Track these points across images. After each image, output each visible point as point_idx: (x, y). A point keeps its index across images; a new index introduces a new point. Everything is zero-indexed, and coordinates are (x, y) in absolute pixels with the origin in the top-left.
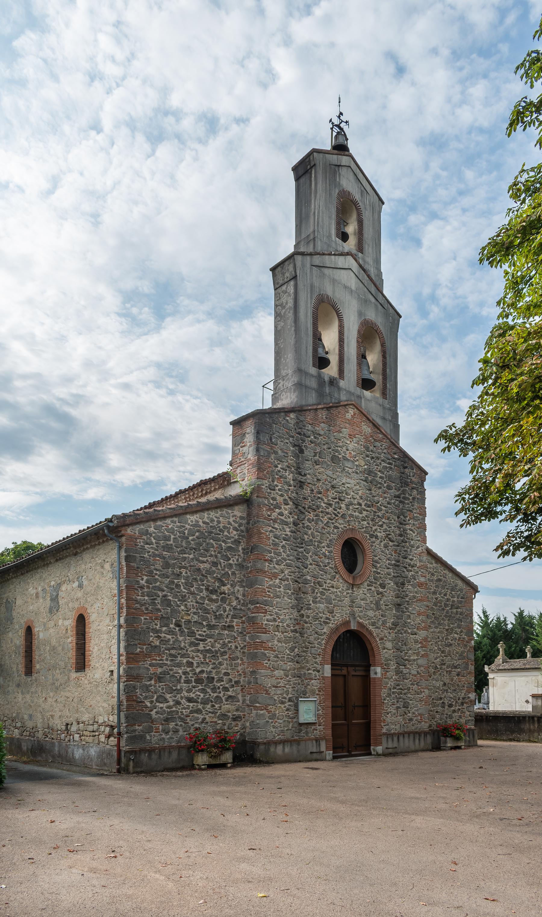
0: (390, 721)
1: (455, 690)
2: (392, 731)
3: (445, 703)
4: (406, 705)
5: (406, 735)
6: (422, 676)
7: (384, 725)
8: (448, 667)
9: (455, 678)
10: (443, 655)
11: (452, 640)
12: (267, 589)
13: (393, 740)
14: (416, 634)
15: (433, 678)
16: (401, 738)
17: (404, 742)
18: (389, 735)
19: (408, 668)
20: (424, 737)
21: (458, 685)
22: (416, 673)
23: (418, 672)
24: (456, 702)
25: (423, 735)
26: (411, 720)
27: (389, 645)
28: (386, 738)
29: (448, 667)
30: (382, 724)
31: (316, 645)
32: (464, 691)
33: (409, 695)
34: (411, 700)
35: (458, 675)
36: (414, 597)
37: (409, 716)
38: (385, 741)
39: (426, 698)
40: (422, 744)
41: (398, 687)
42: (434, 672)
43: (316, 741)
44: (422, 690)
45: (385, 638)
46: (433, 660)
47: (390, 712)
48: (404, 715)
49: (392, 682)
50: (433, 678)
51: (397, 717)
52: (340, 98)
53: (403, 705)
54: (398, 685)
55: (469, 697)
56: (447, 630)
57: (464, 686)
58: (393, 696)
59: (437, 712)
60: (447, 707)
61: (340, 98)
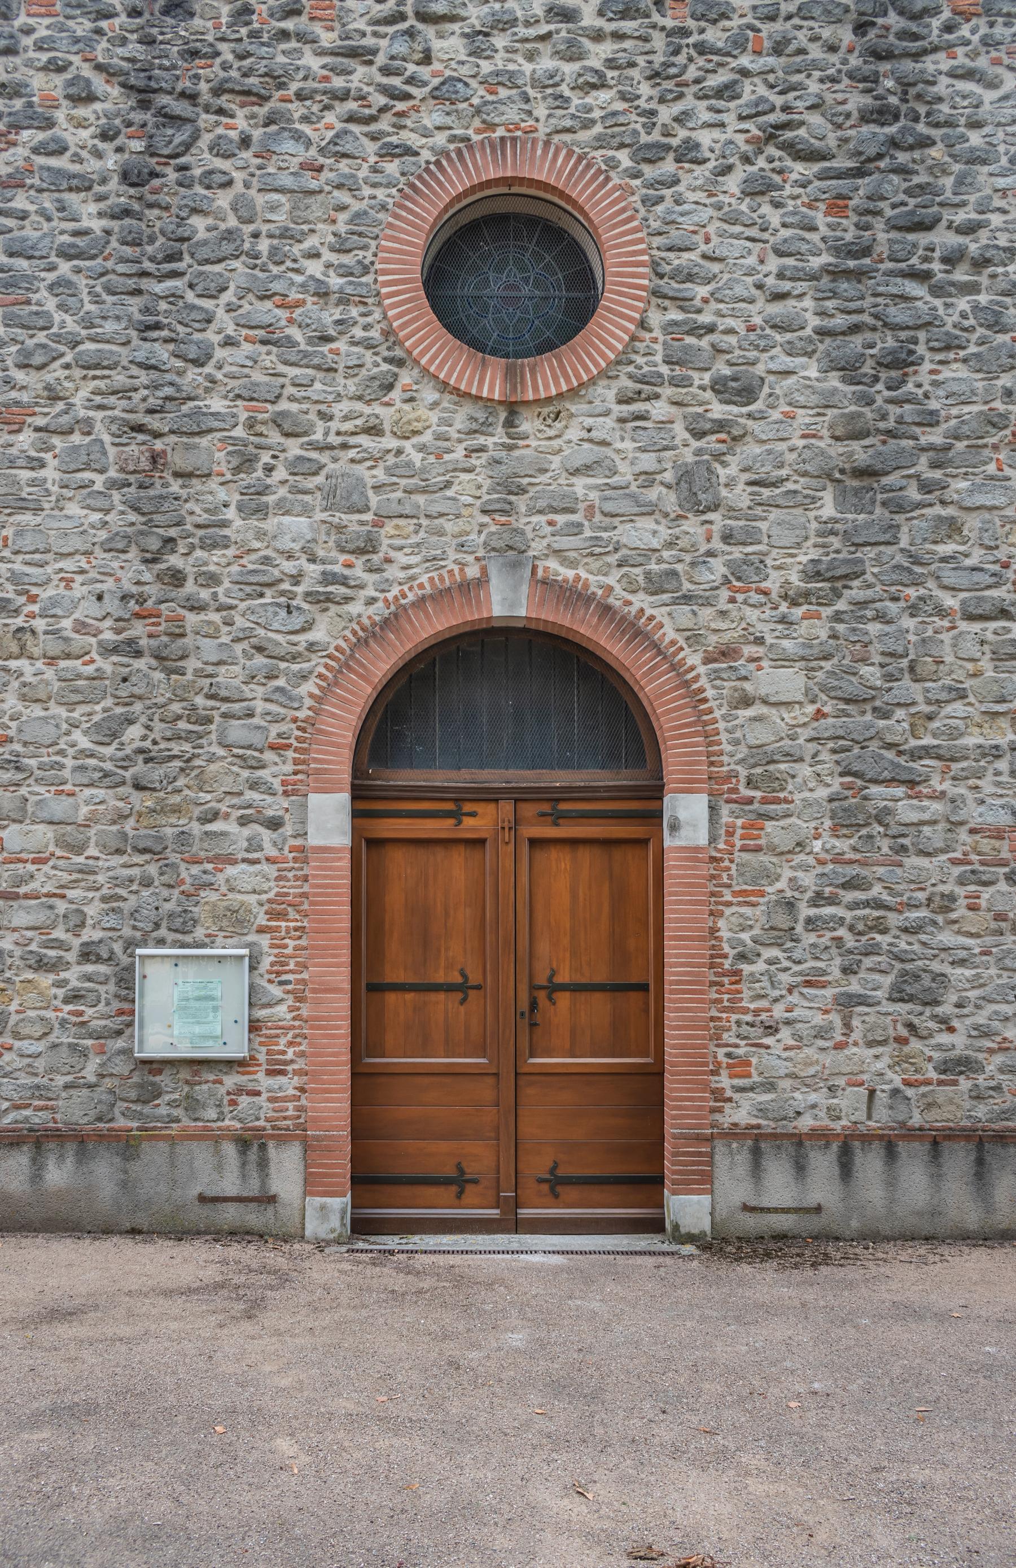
37: (939, 1047)
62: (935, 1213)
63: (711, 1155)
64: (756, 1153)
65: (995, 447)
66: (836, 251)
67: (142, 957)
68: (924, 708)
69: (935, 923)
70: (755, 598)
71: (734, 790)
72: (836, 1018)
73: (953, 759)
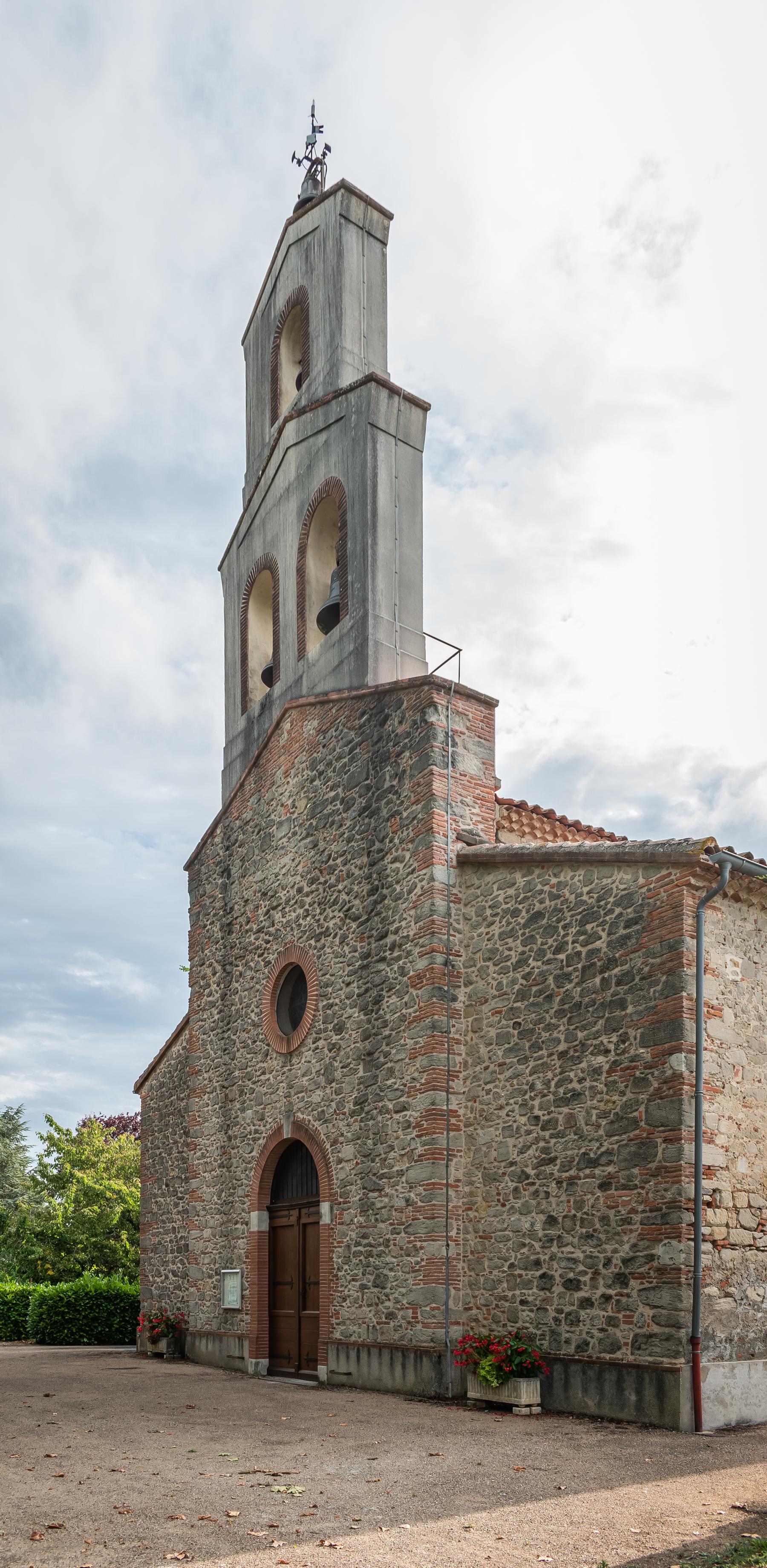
0: (347, 1315)
1: (589, 1236)
2: (353, 1339)
3: (552, 1277)
4: (380, 1283)
5: (374, 1351)
6: (418, 1210)
7: (337, 1324)
8: (564, 1168)
9: (590, 1199)
10: (547, 1134)
11: (580, 1081)
12: (197, 1114)
13: (348, 1357)
14: (404, 1109)
15: (512, 1207)
16: (364, 1355)
17: (369, 1366)
18: (343, 1346)
19: (386, 1195)
20: (415, 1361)
21: (604, 1219)
22: (402, 1203)
23: (407, 1200)
24: (596, 1273)
25: (412, 1356)
26: (391, 1316)
27: (348, 1151)
28: (335, 1352)
29: (564, 1168)
30: (334, 1321)
31: (245, 1181)
32: (630, 1239)
33: (389, 1259)
34: (391, 1270)
35: (604, 1186)
36: (403, 1018)
37: (385, 1308)
38: (335, 1357)
39: (428, 1264)
40: (411, 1377)
41: (365, 1241)
42: (516, 1189)
43: (239, 1338)
44: (418, 1244)
45: (341, 1139)
46: (514, 1156)
47: (349, 1296)
48: (377, 1305)
49: (353, 1230)
50: (512, 1207)
51: (360, 1306)
52: (313, 107)
53: (374, 1282)
54: (364, 1237)
55: (651, 1258)
56: (562, 1055)
57: (627, 1221)
58: (354, 1261)
59: (523, 1302)
60: (558, 1289)
61: (313, 107)
62: (380, 1380)
63: (327, 1350)
64: (380, 1350)
65: (404, 1030)
66: (576, 1184)
67: (224, 1273)
68: (383, 1156)
69: (384, 1252)
70: (342, 1116)
71: (337, 1199)
72: (360, 1294)
73: (390, 1178)
